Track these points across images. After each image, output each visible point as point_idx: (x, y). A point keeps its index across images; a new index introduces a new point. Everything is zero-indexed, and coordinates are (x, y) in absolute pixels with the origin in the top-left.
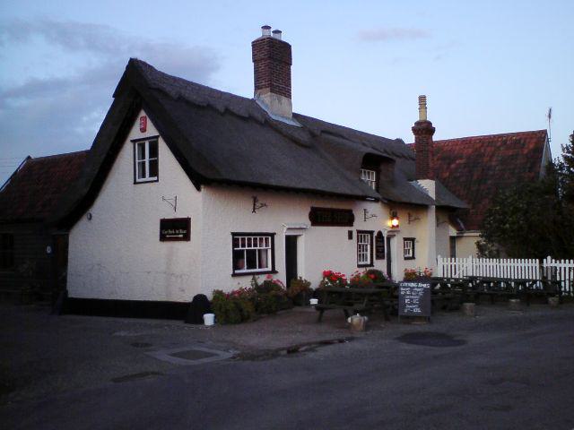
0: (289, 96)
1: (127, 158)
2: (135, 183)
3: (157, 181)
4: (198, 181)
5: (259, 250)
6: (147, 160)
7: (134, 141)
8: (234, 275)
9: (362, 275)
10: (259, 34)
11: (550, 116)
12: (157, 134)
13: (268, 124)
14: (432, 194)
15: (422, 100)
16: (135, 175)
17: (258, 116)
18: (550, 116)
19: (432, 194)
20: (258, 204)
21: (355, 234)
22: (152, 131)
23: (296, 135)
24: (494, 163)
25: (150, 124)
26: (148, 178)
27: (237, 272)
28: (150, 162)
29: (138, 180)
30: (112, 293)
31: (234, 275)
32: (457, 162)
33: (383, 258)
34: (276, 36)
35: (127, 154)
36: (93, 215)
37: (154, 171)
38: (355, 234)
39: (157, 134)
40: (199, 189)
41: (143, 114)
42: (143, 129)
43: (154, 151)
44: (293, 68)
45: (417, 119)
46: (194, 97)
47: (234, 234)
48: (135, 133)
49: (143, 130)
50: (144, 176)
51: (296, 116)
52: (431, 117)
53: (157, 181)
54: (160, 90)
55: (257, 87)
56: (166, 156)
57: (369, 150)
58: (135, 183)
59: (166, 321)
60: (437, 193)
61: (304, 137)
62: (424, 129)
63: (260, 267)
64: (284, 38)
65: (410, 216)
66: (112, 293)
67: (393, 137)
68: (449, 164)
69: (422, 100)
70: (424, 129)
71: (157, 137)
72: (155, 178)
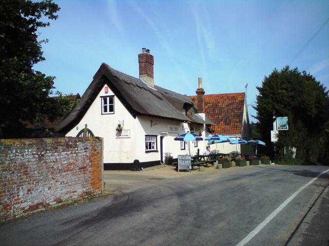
0: (153, 78)
1: (98, 103)
2: (102, 114)
4: (135, 114)
5: (150, 143)
6: (108, 105)
9: (27, 127)
10: (141, 52)
11: (246, 87)
12: (113, 94)
17: (145, 87)
18: (246, 87)
22: (111, 93)
24: (223, 106)
25: (109, 89)
26: (108, 112)
31: (146, 152)
33: (86, 130)
37: (112, 109)
39: (113, 94)
40: (135, 118)
41: (106, 86)
42: (106, 91)
43: (111, 101)
47: (146, 136)
48: (102, 93)
50: (106, 110)
51: (156, 87)
54: (116, 77)
55: (140, 74)
56: (117, 103)
57: (186, 102)
58: (102, 114)
59: (283, 207)
62: (200, 92)
63: (150, 148)
65: (152, 122)
70: (200, 92)
71: (114, 96)
72: (113, 112)
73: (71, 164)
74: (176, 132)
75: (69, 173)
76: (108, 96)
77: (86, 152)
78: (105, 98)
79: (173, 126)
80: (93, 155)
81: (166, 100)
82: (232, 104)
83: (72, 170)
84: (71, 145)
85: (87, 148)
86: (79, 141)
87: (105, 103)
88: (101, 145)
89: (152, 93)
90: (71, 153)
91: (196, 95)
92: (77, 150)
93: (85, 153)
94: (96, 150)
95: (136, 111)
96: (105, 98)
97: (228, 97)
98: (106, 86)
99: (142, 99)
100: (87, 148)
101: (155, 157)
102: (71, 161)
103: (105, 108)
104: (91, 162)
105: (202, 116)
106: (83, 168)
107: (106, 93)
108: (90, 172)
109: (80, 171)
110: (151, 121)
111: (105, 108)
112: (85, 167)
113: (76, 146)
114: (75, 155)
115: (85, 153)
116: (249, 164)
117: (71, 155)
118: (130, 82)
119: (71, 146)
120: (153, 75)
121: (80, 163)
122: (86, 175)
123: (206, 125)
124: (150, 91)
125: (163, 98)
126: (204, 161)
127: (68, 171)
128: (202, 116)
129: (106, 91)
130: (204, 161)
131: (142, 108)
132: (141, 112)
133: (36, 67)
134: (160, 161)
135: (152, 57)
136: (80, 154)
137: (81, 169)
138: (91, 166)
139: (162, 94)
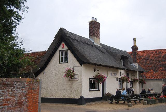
0: (99, 38)
1: (57, 55)
2: (60, 63)
3: (67, 63)
7: (60, 51)
8: (90, 91)
10: (91, 20)
12: (68, 49)
13: (93, 46)
14: (138, 68)
15: (134, 39)
16: (60, 61)
19: (138, 68)
20: (96, 70)
21: (118, 79)
22: (66, 48)
23: (102, 49)
25: (65, 46)
26: (64, 62)
27: (90, 90)
28: (65, 57)
29: (61, 62)
30: (51, 96)
31: (90, 91)
32: (142, 58)
34: (95, 20)
35: (57, 54)
36: (45, 72)
37: (66, 59)
38: (118, 79)
39: (68, 49)
40: (82, 65)
41: (63, 43)
42: (63, 47)
43: (66, 54)
44: (100, 30)
45: (133, 45)
46: (77, 39)
48: (60, 48)
49: (63, 48)
50: (62, 61)
51: (101, 44)
52: (137, 44)
53: (67, 63)
56: (70, 55)
57: (123, 55)
60: (139, 67)
61: (104, 51)
62: (135, 48)
63: (94, 88)
64: (98, 21)
66: (51, 96)
67: (124, 50)
68: (139, 59)
69: (134, 39)
70: (135, 48)
71: (68, 50)
72: (67, 62)
73: (7, 100)
74: (115, 76)
75: (5, 107)
76: (64, 50)
77: (22, 90)
78: (62, 52)
79: (113, 73)
80: (29, 93)
81: (108, 54)
82: (159, 57)
83: (8, 105)
84: (8, 84)
85: (24, 87)
86: (16, 81)
87: (62, 55)
88: (38, 85)
89: (98, 49)
90: (8, 91)
91: (131, 50)
92: (14, 88)
93: (21, 91)
94: (33, 89)
95: (82, 61)
96: (62, 52)
97: (156, 53)
98: (63, 43)
99: (86, 52)
100: (24, 87)
101: (98, 94)
102: (8, 97)
103: (62, 58)
104: (28, 98)
105: (137, 65)
106: (20, 103)
107: (63, 48)
108: (27, 106)
109: (16, 106)
110: (95, 68)
111: (62, 58)
112: (22, 103)
113: (13, 85)
114: (11, 92)
115: (21, 91)
116: (147, 103)
117: (7, 93)
118: (81, 40)
119: (8, 85)
120: (99, 36)
121: (16, 99)
122: (22, 109)
123: (139, 72)
124: (96, 47)
125: (106, 53)
126: (26, 98)
127: (4, 105)
128: (137, 65)
129: (63, 47)
130: (26, 98)
131: (86, 59)
132: (85, 61)
133: (138, 50)
134: (101, 98)
135: (98, 24)
136: (16, 92)
137: (17, 103)
138: (28, 102)
139: (106, 50)
